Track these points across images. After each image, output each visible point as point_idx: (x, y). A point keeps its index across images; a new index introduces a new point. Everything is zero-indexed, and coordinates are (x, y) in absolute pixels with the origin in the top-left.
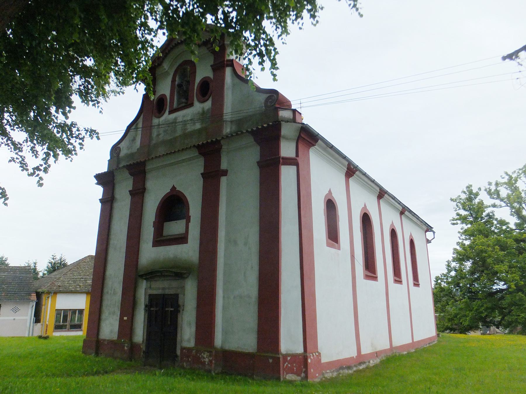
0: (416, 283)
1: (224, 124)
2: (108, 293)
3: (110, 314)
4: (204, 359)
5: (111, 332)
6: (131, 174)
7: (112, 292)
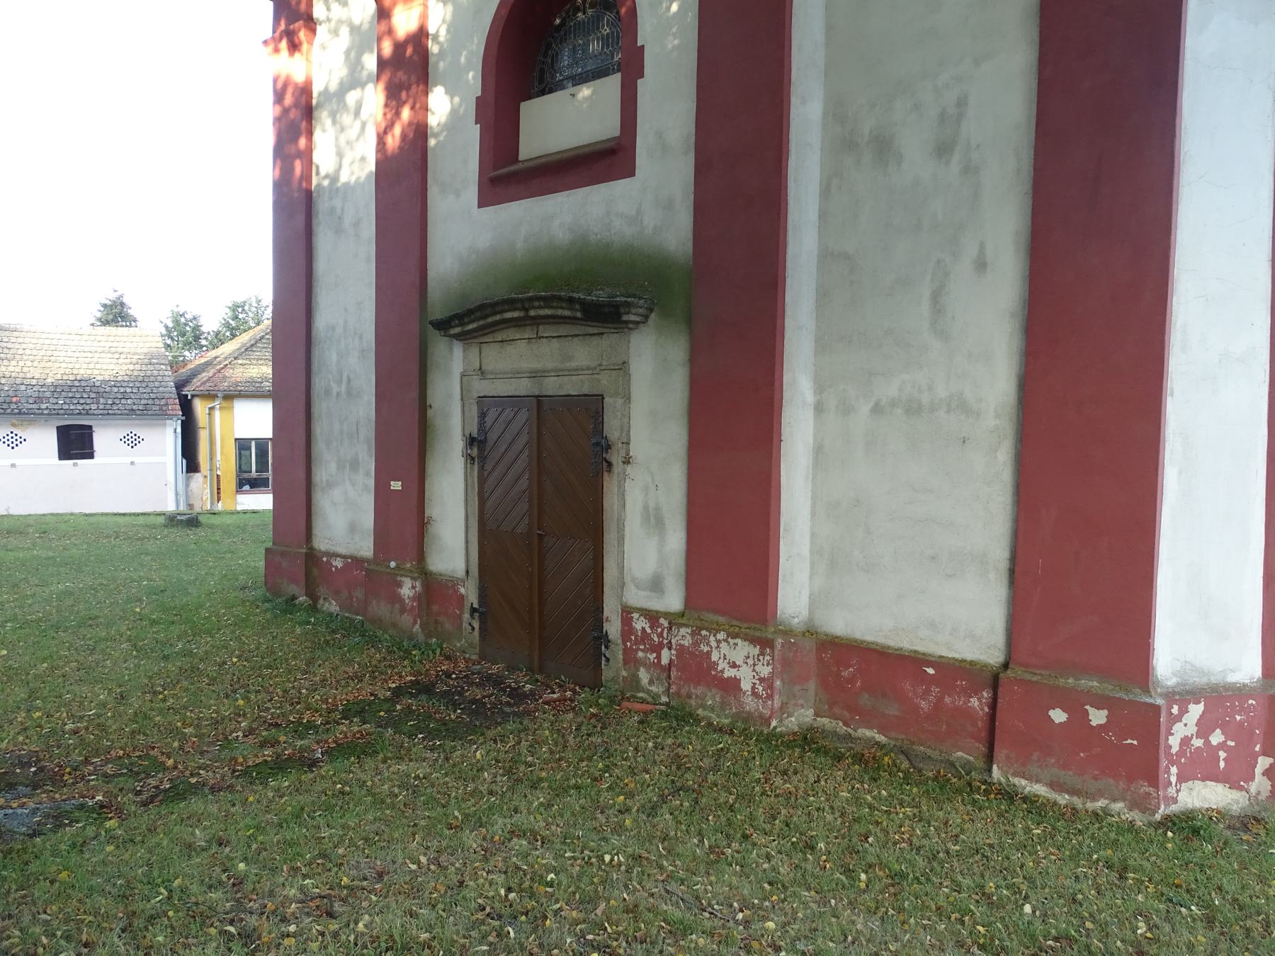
2: (328, 392)
3: (341, 467)
5: (353, 528)
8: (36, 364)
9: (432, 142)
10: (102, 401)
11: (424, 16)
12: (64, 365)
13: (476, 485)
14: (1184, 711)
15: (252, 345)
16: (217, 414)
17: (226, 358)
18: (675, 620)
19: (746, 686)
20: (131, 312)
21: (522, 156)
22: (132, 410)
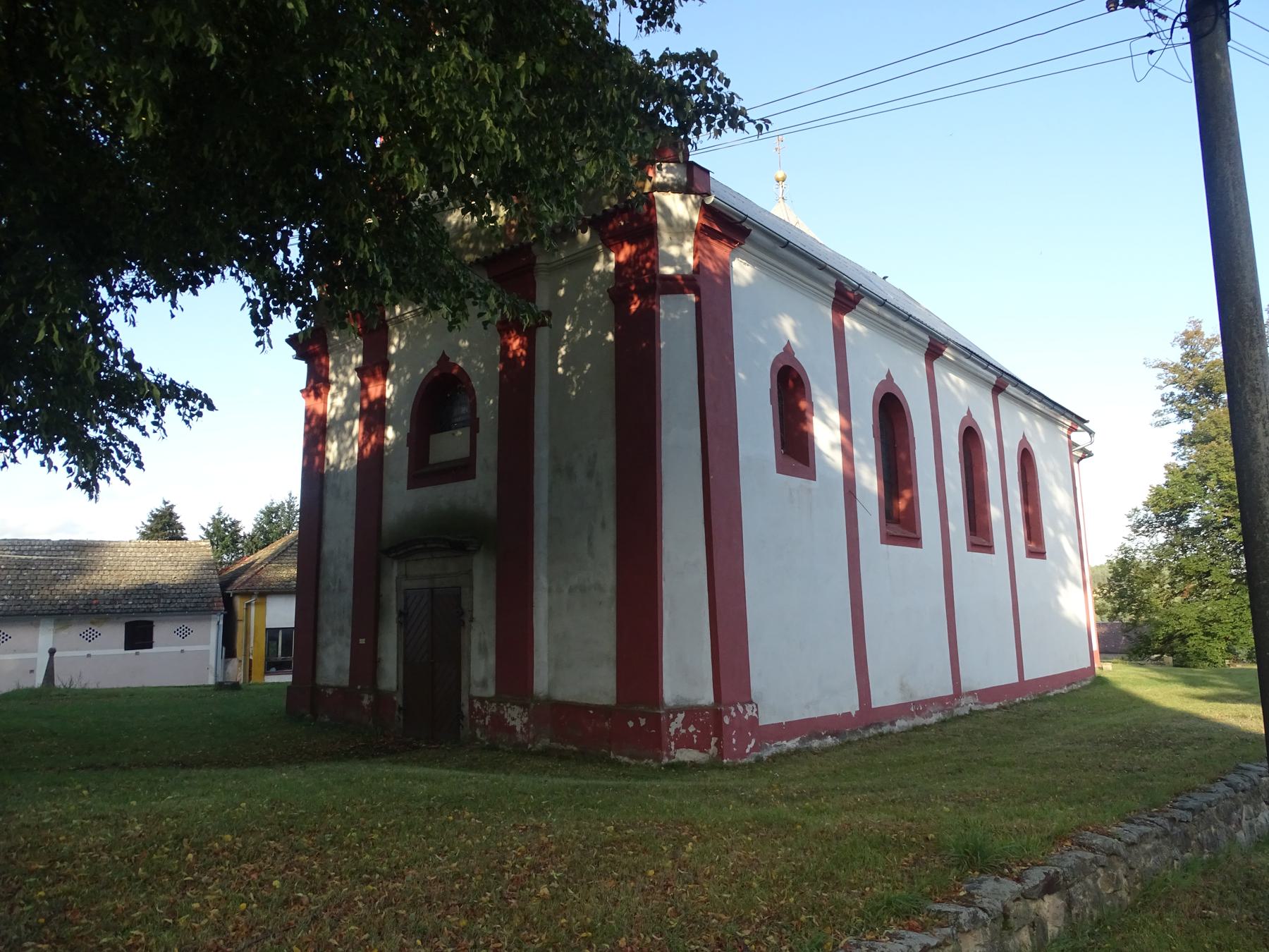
0: (1037, 549)
8: (112, 572)
9: (386, 454)
10: (162, 600)
11: (384, 391)
12: (134, 573)
14: (675, 717)
15: (283, 551)
16: (253, 609)
17: (261, 563)
18: (491, 700)
19: (518, 729)
20: (179, 521)
21: (431, 461)
22: (186, 607)
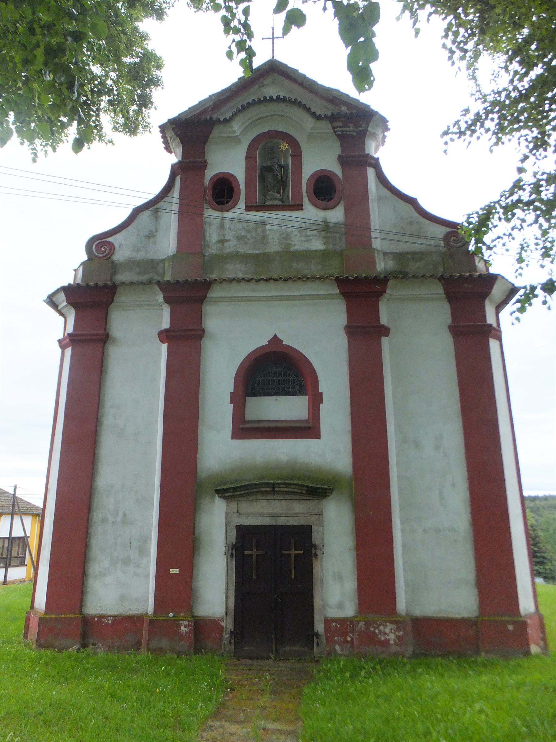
1: (376, 255)
2: (105, 521)
4: (386, 637)
6: (167, 300)
7: (119, 519)
13: (234, 567)
